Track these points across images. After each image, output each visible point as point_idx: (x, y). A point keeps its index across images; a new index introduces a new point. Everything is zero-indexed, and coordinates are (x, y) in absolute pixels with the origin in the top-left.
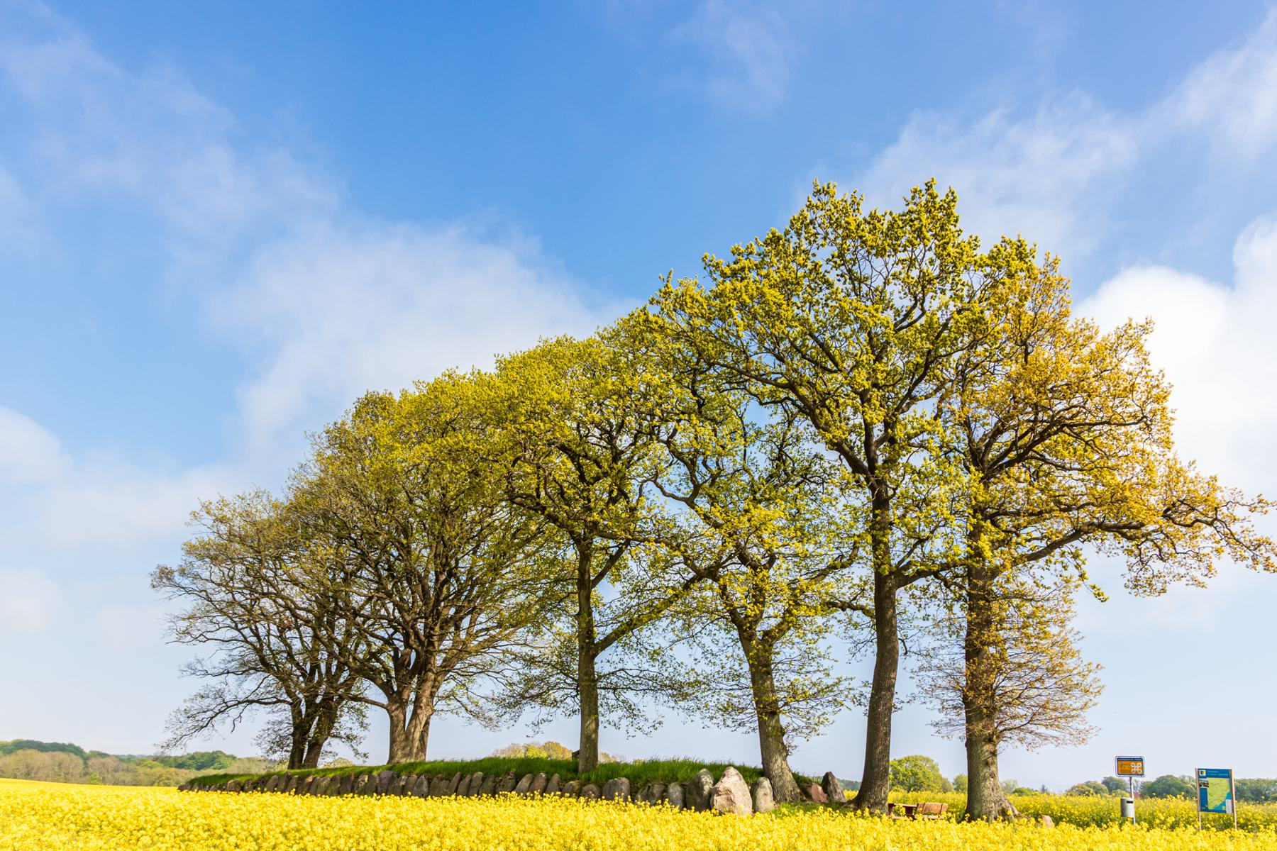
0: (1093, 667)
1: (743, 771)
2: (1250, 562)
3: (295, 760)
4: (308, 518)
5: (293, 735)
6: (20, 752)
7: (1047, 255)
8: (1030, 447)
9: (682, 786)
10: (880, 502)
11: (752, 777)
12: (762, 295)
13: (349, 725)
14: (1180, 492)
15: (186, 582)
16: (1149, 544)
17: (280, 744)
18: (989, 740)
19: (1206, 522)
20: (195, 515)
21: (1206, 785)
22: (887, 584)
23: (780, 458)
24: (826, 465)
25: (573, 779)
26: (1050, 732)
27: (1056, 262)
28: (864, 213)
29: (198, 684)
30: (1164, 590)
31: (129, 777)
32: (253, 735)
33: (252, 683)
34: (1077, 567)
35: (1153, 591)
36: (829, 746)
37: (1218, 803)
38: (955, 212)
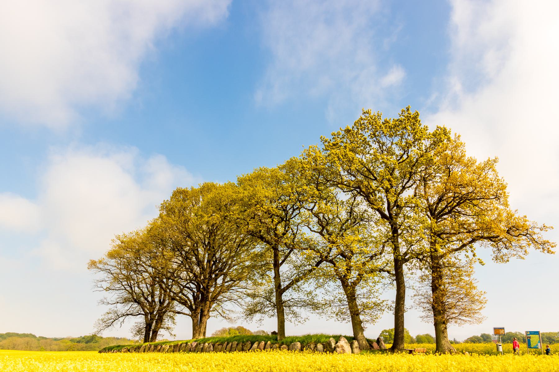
0: (483, 293)
2: (542, 250)
3: (146, 340)
7: (455, 134)
9: (323, 345)
10: (395, 231)
11: (350, 340)
12: (346, 154)
14: (512, 222)
15: (101, 266)
16: (501, 243)
17: (139, 331)
18: (444, 323)
19: (524, 235)
21: (530, 338)
22: (398, 263)
23: (351, 212)
24: (369, 214)
25: (276, 343)
26: (467, 319)
27: (459, 136)
28: (382, 120)
29: (107, 308)
30: (508, 261)
32: (129, 328)
34: (472, 251)
35: (503, 261)
36: (378, 326)
38: (419, 119)
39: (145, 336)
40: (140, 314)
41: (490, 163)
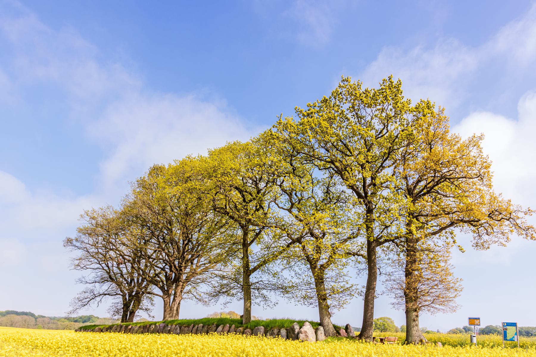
1: (312, 323)
2: (525, 236)
3: (124, 319)
4: (130, 217)
5: (123, 308)
6: (9, 315)
7: (440, 107)
8: (432, 188)
9: (286, 330)
10: (370, 211)
11: (316, 326)
12: (320, 124)
13: (146, 304)
14: (495, 206)
15: (78, 244)
16: (482, 228)
17: (118, 312)
18: (416, 311)
20: (82, 216)
21: (506, 329)
22: (372, 246)
23: (328, 192)
25: (240, 327)
26: (441, 307)
27: (443, 110)
28: (363, 89)
29: (83, 287)
30: (488, 248)
31: (54, 326)
32: (106, 308)
33: (106, 287)
34: (452, 238)
35: (484, 248)
36: (348, 313)
37: (511, 337)
39: (123, 317)
40: (117, 294)
41: (475, 139)
